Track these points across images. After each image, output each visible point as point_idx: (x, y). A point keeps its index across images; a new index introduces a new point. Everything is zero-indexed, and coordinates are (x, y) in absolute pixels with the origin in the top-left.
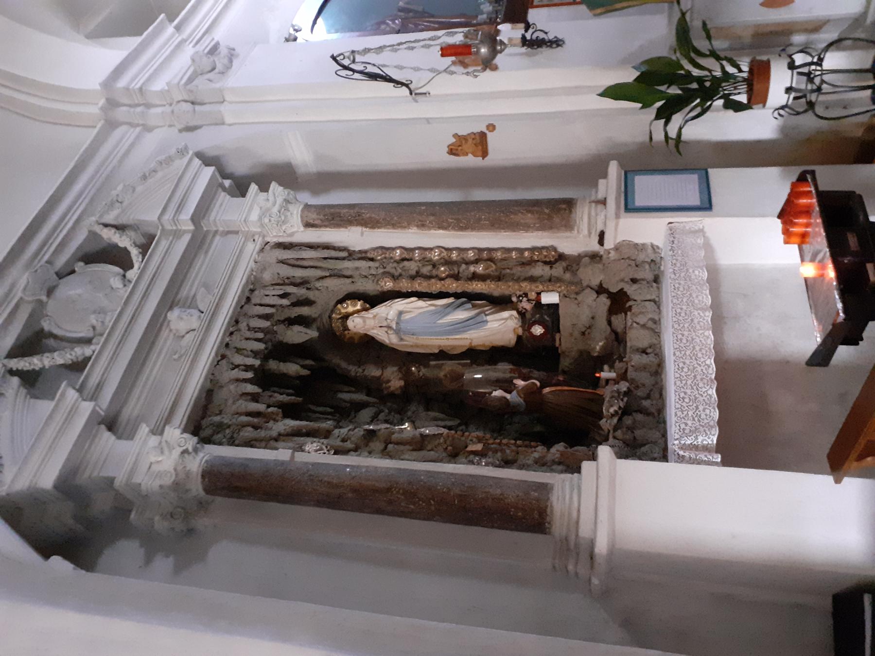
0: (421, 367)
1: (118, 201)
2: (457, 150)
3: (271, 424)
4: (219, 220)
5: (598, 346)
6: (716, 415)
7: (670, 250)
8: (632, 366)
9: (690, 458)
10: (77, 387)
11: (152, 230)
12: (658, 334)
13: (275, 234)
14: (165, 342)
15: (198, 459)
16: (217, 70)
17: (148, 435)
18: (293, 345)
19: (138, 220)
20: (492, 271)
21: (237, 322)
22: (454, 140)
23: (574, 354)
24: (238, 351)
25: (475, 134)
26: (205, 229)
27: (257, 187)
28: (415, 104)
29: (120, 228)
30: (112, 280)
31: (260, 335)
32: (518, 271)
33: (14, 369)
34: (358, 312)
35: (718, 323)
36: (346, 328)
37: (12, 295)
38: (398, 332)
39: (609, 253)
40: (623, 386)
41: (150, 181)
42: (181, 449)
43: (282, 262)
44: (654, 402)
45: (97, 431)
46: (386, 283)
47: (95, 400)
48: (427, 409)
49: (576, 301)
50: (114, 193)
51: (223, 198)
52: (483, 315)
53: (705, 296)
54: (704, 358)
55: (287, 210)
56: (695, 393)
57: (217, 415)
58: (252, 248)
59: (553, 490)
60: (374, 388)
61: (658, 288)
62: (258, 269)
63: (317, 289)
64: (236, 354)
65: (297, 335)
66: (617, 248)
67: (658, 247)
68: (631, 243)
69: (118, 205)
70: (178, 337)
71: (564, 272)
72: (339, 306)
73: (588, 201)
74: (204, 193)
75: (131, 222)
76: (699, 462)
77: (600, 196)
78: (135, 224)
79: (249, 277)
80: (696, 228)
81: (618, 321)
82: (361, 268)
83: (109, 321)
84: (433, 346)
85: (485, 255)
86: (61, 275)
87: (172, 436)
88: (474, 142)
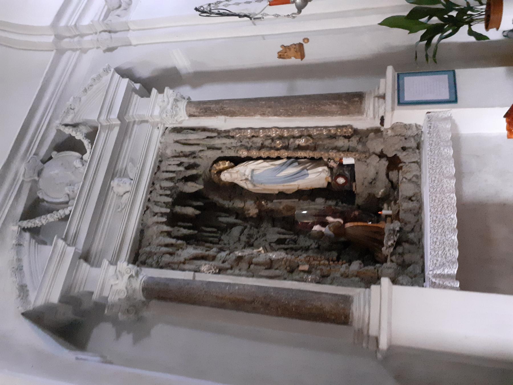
0: (268, 201)
1: (71, 109)
2: (284, 55)
3: (180, 252)
4: (135, 115)
5: (380, 192)
6: (457, 254)
7: (428, 133)
8: (403, 210)
9: (439, 284)
10: (64, 237)
11: (95, 124)
12: (418, 185)
13: (170, 122)
14: (112, 200)
15: (139, 280)
16: (122, 8)
17: (108, 265)
18: (188, 193)
19: (86, 120)
20: (311, 144)
21: (153, 184)
22: (281, 49)
23: (365, 195)
24: (156, 203)
25: (295, 45)
26: (127, 121)
27: (156, 91)
28: (254, 26)
29: (75, 126)
30: (75, 163)
31: (168, 192)
32: (327, 142)
33: (26, 227)
34: (227, 168)
35: (459, 176)
36: (220, 180)
37: (18, 178)
38: (252, 182)
39: (387, 132)
40: (397, 225)
41: (89, 92)
42: (129, 275)
43: (177, 142)
44: (416, 234)
45: (79, 263)
46: (242, 153)
47: (75, 246)
48: (274, 226)
49: (366, 164)
50: (68, 103)
51: (136, 97)
52: (305, 170)
53: (451, 168)
54: (450, 214)
55: (177, 106)
56: (443, 217)
57: (147, 246)
58: (157, 134)
59: (353, 302)
60: (240, 214)
61: (419, 153)
62: (162, 148)
63: (200, 157)
64: (155, 206)
65: (191, 187)
66: (392, 128)
67: (420, 126)
68: (402, 124)
69: (72, 111)
70: (119, 196)
71: (358, 143)
72: (215, 165)
73: (373, 96)
74: (124, 98)
75: (81, 121)
76: (445, 287)
77: (381, 92)
78: (84, 122)
79: (158, 154)
80: (446, 116)
81: (393, 175)
82: (226, 143)
83: (77, 188)
84: (276, 190)
85: (306, 133)
86: (44, 162)
87: (122, 267)
88: (295, 50)
